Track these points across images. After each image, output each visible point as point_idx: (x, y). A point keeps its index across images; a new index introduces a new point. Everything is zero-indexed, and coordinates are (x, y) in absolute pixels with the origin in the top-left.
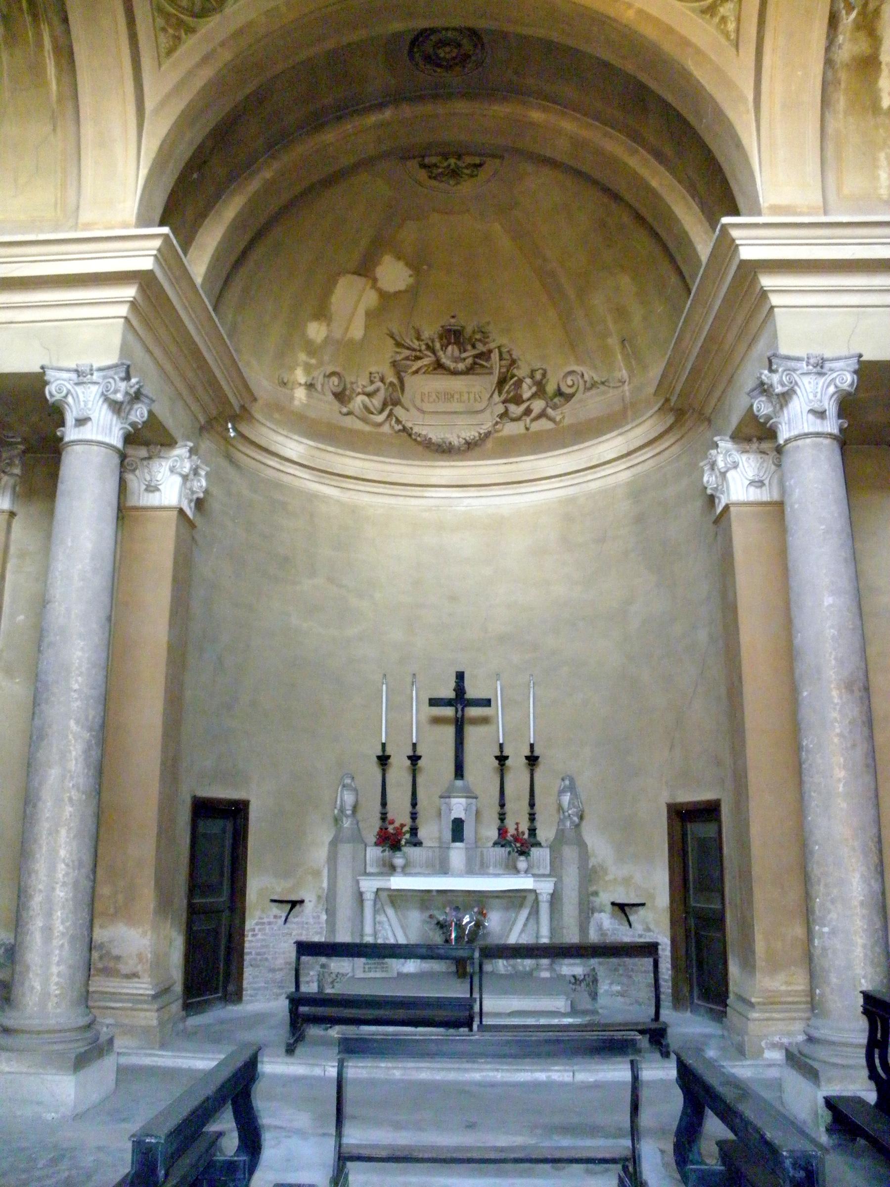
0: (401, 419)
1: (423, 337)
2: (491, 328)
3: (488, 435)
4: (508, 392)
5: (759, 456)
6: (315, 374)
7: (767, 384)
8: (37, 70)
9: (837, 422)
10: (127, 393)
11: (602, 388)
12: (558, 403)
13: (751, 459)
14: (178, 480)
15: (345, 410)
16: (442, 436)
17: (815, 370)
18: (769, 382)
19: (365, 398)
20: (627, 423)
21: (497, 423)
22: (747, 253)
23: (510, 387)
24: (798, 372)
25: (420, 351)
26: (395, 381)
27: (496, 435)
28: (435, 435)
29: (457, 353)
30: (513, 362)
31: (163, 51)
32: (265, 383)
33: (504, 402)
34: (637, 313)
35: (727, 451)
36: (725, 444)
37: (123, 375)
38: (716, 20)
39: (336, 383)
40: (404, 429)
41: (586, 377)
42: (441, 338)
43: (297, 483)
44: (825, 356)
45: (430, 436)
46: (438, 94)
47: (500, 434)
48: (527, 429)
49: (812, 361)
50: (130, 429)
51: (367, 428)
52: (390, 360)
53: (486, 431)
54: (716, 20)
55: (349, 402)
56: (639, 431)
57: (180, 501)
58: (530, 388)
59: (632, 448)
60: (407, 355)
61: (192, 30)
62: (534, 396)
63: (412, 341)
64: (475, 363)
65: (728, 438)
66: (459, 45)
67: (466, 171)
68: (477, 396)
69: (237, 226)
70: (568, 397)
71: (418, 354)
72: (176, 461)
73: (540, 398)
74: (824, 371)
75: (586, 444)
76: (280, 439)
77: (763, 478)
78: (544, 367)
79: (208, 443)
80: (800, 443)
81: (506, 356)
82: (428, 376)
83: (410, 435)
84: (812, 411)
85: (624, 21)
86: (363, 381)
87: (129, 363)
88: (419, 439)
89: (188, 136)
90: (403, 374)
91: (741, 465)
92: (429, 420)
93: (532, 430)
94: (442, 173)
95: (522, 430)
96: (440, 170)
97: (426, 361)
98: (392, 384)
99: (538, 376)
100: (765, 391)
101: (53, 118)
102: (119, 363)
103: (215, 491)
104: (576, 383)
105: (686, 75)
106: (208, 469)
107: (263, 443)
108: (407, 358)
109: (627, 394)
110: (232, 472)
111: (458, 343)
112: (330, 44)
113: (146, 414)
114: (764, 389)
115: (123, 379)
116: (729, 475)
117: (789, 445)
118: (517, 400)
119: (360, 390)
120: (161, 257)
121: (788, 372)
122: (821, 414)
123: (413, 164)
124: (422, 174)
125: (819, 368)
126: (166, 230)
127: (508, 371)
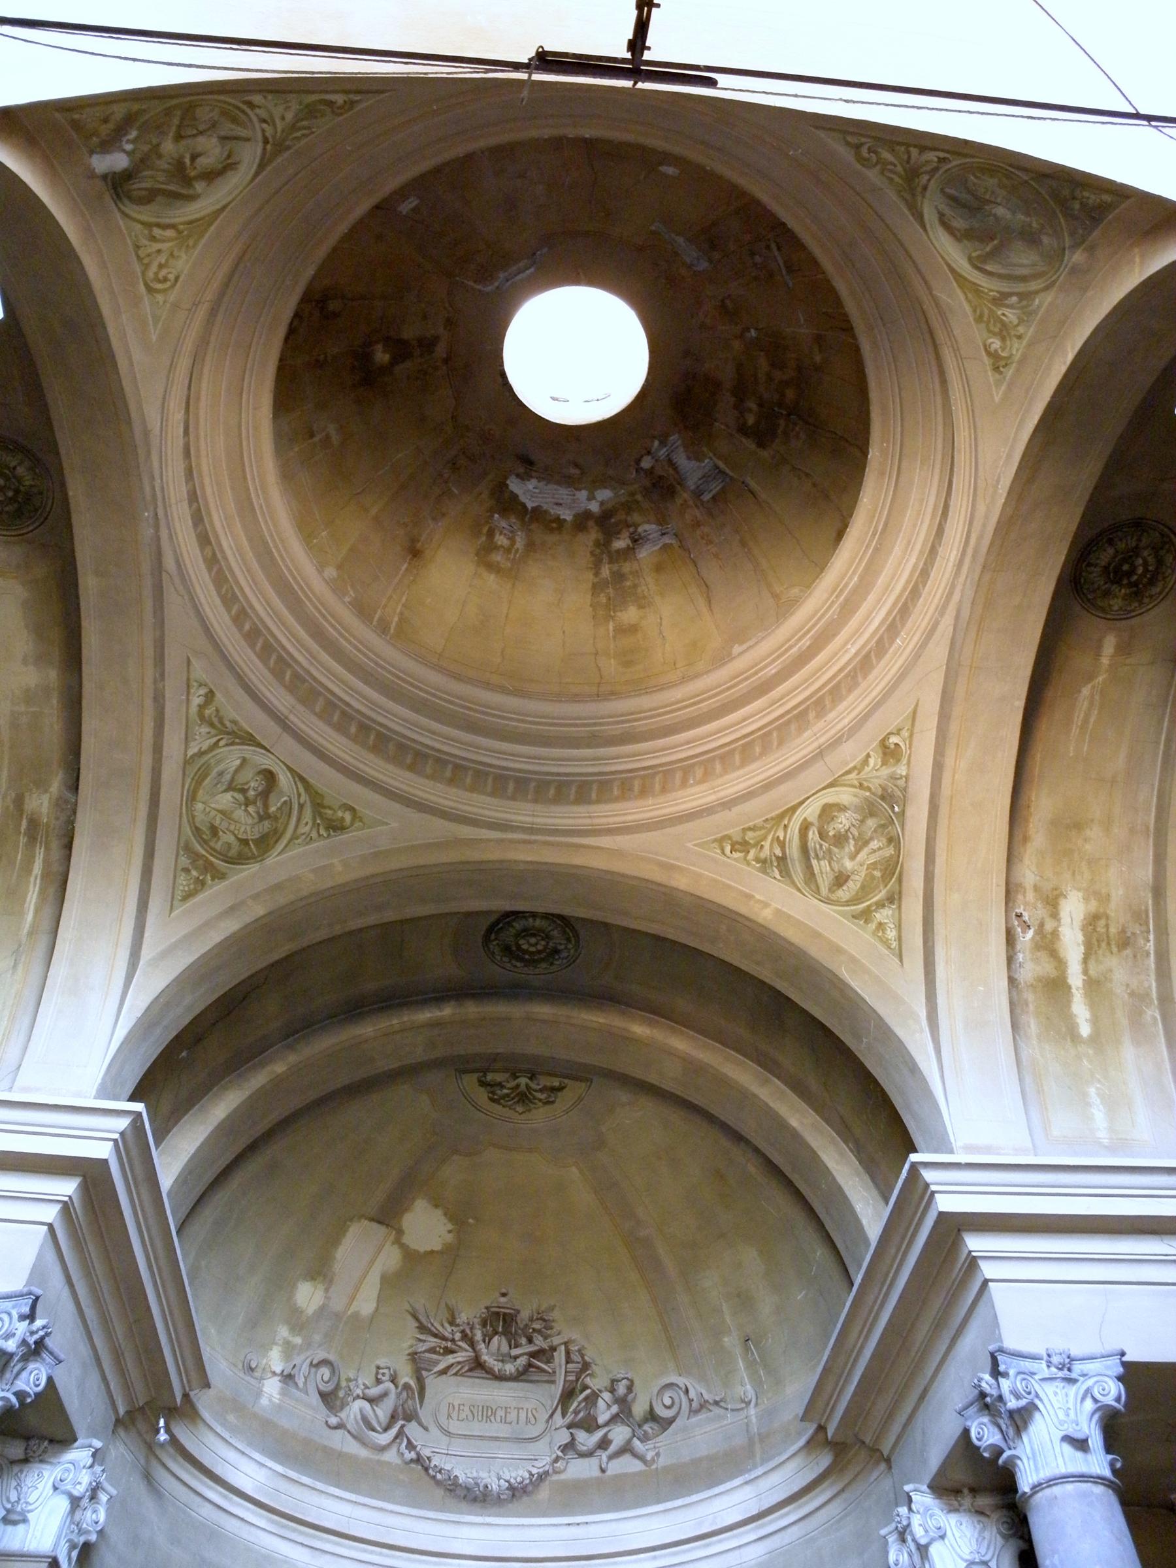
0: (415, 1443)
1: (458, 1321)
2: (555, 1314)
3: (542, 1477)
4: (576, 1412)
5: (976, 1518)
6: (297, 1360)
7: (992, 1396)
8: (15, 895)
9: (1106, 1459)
10: (24, 1342)
11: (717, 1410)
12: (650, 1431)
13: (964, 1524)
14: (64, 1504)
15: (333, 1421)
16: (475, 1475)
17: (1060, 1374)
18: (995, 1393)
19: (366, 1405)
20: (755, 1467)
21: (557, 1460)
22: (946, 1203)
23: (580, 1403)
24: (1036, 1377)
25: (453, 1340)
26: (412, 1383)
27: (555, 1477)
28: (464, 1472)
29: (505, 1348)
30: (586, 1366)
31: (179, 895)
32: (223, 1365)
33: (569, 1427)
34: (766, 1304)
35: (927, 1509)
36: (923, 1499)
37: (26, 1310)
38: (872, 926)
39: (326, 1378)
40: (418, 1460)
41: (692, 1394)
42: (484, 1324)
43: (245, 1532)
44: (1073, 1353)
45: (456, 1472)
46: (515, 991)
47: (563, 1477)
48: (603, 1471)
49: (1055, 1360)
50: (14, 1399)
51: (364, 1453)
52: (410, 1351)
53: (541, 1470)
54: (872, 926)
55: (342, 1408)
56: (775, 1478)
57: (56, 1544)
58: (609, 1406)
59: (766, 1504)
60: (433, 1345)
61: (220, 876)
62: (614, 1419)
63: (442, 1326)
64: (530, 1365)
65: (924, 1488)
66: (548, 937)
67: (538, 1095)
68: (530, 1415)
69: (226, 1129)
70: (665, 1424)
71: (449, 1344)
72: (68, 1470)
73: (623, 1422)
74: (1074, 1375)
75: (695, 1498)
76: (231, 1455)
77: (987, 1558)
78: (629, 1376)
79: (122, 1448)
80: (1057, 1490)
81: (576, 1357)
82: (459, 1378)
83: (426, 1469)
84: (1068, 1439)
85: (760, 921)
86: (367, 1378)
87: (39, 1292)
88: (439, 1476)
89: (188, 1000)
90: (424, 1373)
91: (949, 1533)
92: (458, 1447)
93: (609, 1473)
94: (507, 1095)
95: (596, 1473)
96: (506, 1091)
97: (460, 1357)
98: (406, 1387)
99: (621, 1389)
100: (987, 1406)
101: (64, 835)
102: (26, 1290)
103: (115, 1535)
104: (677, 1401)
105: (842, 987)
106: (114, 1492)
107: (206, 1461)
108: (432, 1350)
109: (754, 1420)
110: (148, 1505)
111: (506, 1333)
112: (390, 916)
113: (43, 1382)
114: (986, 1404)
115: (22, 1318)
116: (934, 1550)
117: (1040, 1495)
118: (589, 1425)
119: (359, 1392)
120: (122, 1145)
121: (1023, 1376)
122: (1081, 1444)
123: (470, 1081)
124: (482, 1095)
125: (1066, 1371)
126: (139, 1107)
127: (577, 1380)
